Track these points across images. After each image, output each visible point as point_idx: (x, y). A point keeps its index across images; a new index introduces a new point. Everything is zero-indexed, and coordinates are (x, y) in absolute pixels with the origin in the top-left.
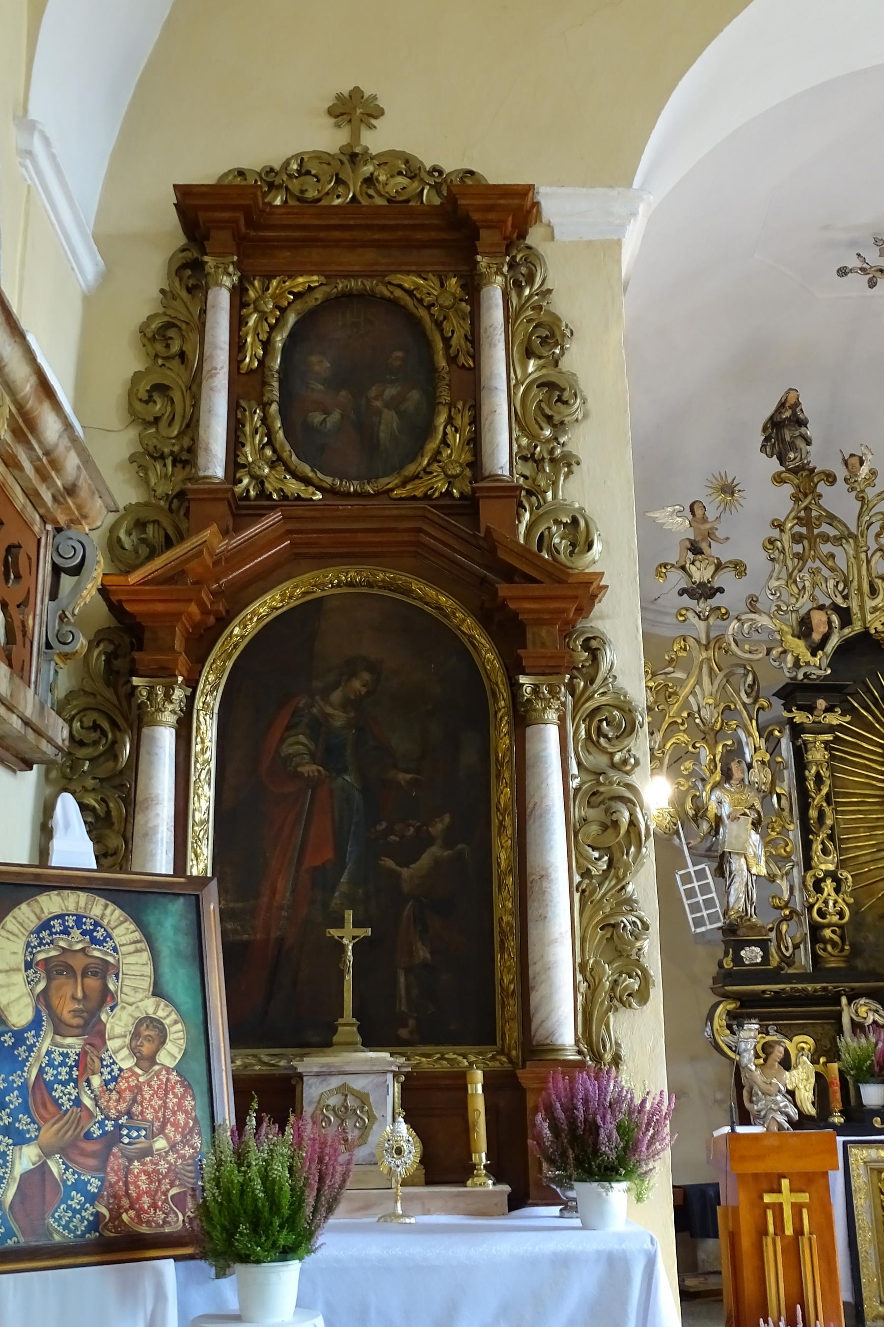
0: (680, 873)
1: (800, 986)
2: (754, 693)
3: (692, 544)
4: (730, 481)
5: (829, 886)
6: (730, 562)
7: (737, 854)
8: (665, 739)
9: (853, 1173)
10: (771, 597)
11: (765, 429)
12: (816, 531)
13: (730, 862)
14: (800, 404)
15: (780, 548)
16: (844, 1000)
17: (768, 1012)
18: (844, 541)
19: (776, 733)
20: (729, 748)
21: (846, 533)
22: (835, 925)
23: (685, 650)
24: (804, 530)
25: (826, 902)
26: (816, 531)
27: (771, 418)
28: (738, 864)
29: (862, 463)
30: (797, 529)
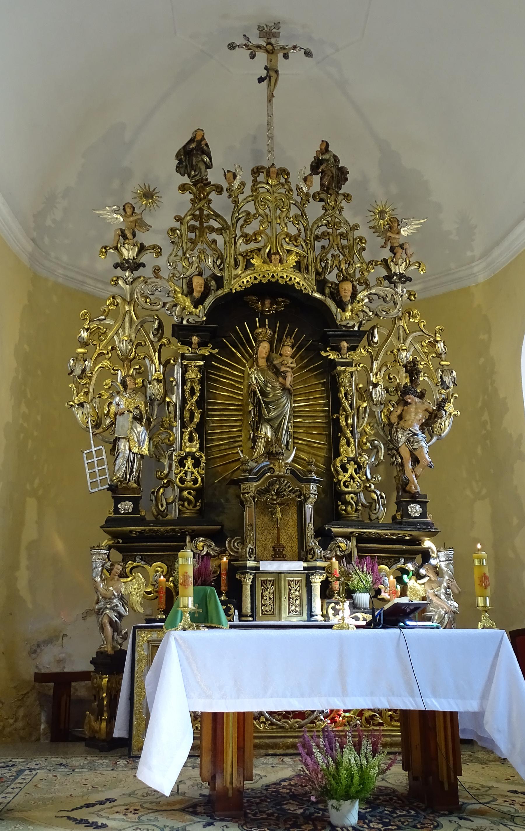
0: (86, 452)
1: (155, 528)
2: (159, 335)
3: (122, 232)
4: (151, 190)
5: (189, 463)
6: (150, 246)
7: (124, 438)
8: (95, 364)
9: (138, 649)
10: (169, 267)
11: (177, 156)
12: (205, 225)
13: (118, 445)
14: (204, 139)
15: (179, 235)
16: (188, 539)
17: (133, 546)
18: (223, 232)
19: (172, 361)
20: (138, 371)
21: (225, 226)
22: (191, 488)
23: (114, 305)
24: (197, 224)
25: (186, 473)
26: (205, 225)
27: (184, 147)
28: (123, 446)
29: (235, 176)
30: (193, 222)
